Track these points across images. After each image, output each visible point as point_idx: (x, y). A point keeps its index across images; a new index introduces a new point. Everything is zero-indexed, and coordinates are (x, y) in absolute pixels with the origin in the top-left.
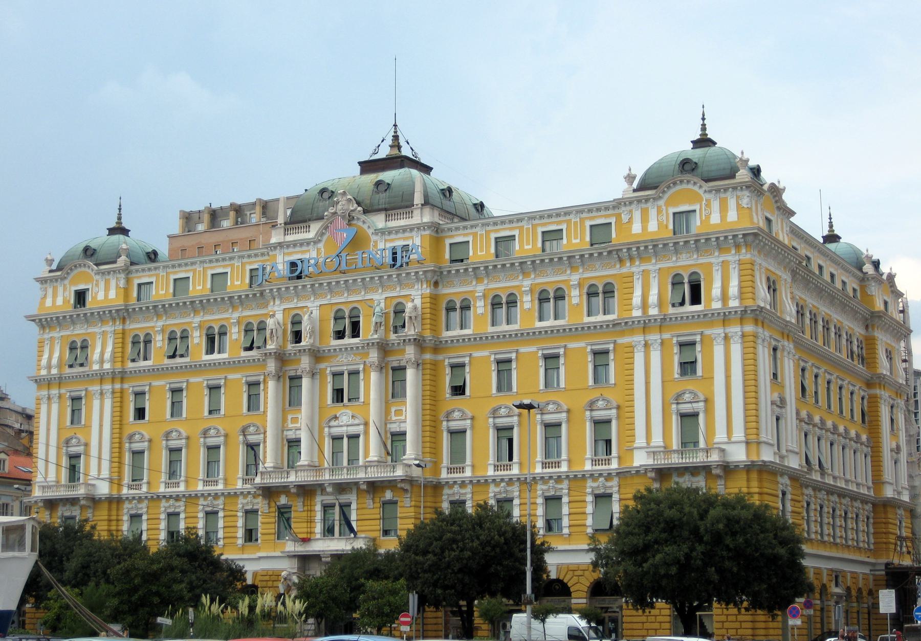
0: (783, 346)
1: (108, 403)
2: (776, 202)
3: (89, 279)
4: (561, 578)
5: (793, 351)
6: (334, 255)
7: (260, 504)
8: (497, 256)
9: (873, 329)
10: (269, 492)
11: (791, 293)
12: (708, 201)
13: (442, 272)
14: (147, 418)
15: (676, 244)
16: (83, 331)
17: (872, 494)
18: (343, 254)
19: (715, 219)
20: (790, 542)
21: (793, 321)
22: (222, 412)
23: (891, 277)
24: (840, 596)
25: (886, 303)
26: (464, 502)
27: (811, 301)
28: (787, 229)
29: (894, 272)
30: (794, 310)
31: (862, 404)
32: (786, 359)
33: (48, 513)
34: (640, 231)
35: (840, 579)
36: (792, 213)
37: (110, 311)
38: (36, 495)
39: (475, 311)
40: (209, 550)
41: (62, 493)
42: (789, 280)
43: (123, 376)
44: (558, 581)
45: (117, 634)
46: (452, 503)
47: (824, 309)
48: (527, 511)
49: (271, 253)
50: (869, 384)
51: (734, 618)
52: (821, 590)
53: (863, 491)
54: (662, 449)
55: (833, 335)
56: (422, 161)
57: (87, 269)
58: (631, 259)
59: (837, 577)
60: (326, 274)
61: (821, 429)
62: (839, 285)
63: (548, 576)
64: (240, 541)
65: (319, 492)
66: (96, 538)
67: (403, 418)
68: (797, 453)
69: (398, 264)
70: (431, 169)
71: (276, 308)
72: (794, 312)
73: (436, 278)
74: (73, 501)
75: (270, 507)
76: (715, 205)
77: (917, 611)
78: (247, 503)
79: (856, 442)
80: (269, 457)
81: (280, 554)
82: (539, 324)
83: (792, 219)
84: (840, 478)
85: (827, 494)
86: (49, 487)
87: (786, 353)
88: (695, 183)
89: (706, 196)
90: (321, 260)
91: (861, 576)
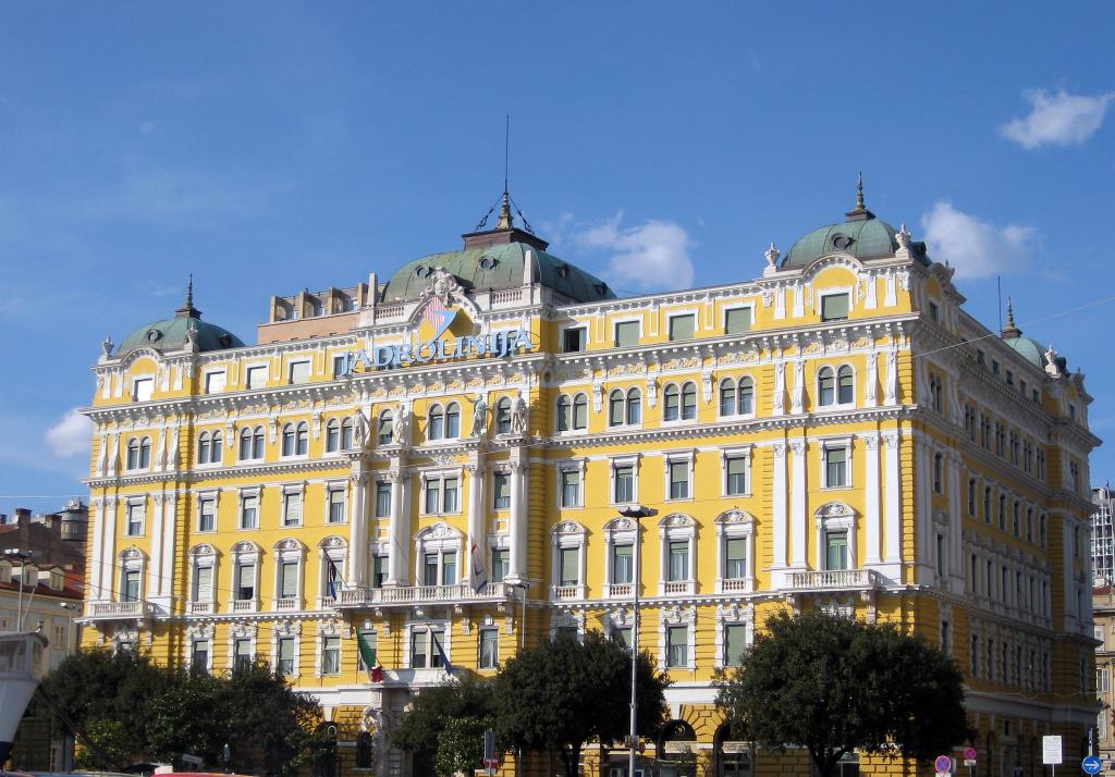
0: (948, 453)
1: (170, 509)
2: (943, 285)
3: (850, 279)
4: (685, 719)
5: (960, 460)
6: (432, 341)
7: (342, 628)
8: (671, 338)
9: (1057, 439)
10: (354, 616)
11: (959, 392)
12: (103, 379)
13: (554, 363)
14: (748, 490)
15: (824, 333)
16: (145, 428)
17: (1051, 628)
18: (441, 341)
19: (870, 304)
20: (949, 678)
21: (961, 424)
22: (300, 522)
23: (1079, 379)
24: (1009, 746)
25: (1072, 408)
26: (576, 629)
27: (983, 403)
28: (955, 317)
29: (1082, 372)
30: (962, 415)
31: (1042, 525)
32: (951, 468)
33: (102, 635)
34: (108, 397)
35: (1011, 726)
36: (962, 300)
37: (175, 405)
38: (88, 615)
39: (592, 409)
40: (280, 680)
41: (118, 614)
42: (957, 377)
43: (810, 422)
44: (681, 722)
45: (195, 768)
46: (561, 629)
47: (998, 413)
48: (649, 640)
49: (358, 339)
50: (1049, 502)
51: (882, 769)
52: (988, 738)
53: (1041, 624)
54: (394, 587)
55: (1008, 443)
56: (537, 236)
57: (146, 357)
58: (772, 349)
59: (1007, 723)
60: (421, 364)
61: (992, 551)
62: (1017, 385)
63: (668, 715)
64: (318, 673)
65: (408, 617)
66: (151, 663)
67: (507, 530)
68: (962, 578)
69: (504, 352)
71: (363, 403)
72: (962, 416)
73: (547, 370)
74: (129, 624)
75: (352, 633)
76: (871, 287)
77: (1086, 762)
78: (672, 616)
79: (1033, 568)
80: (349, 576)
81: (362, 687)
82: (239, 463)
83: (961, 307)
84: (999, 605)
85: (1012, 631)
86: (105, 606)
87: (950, 462)
88: (848, 262)
90: (415, 348)
91: (1021, 722)
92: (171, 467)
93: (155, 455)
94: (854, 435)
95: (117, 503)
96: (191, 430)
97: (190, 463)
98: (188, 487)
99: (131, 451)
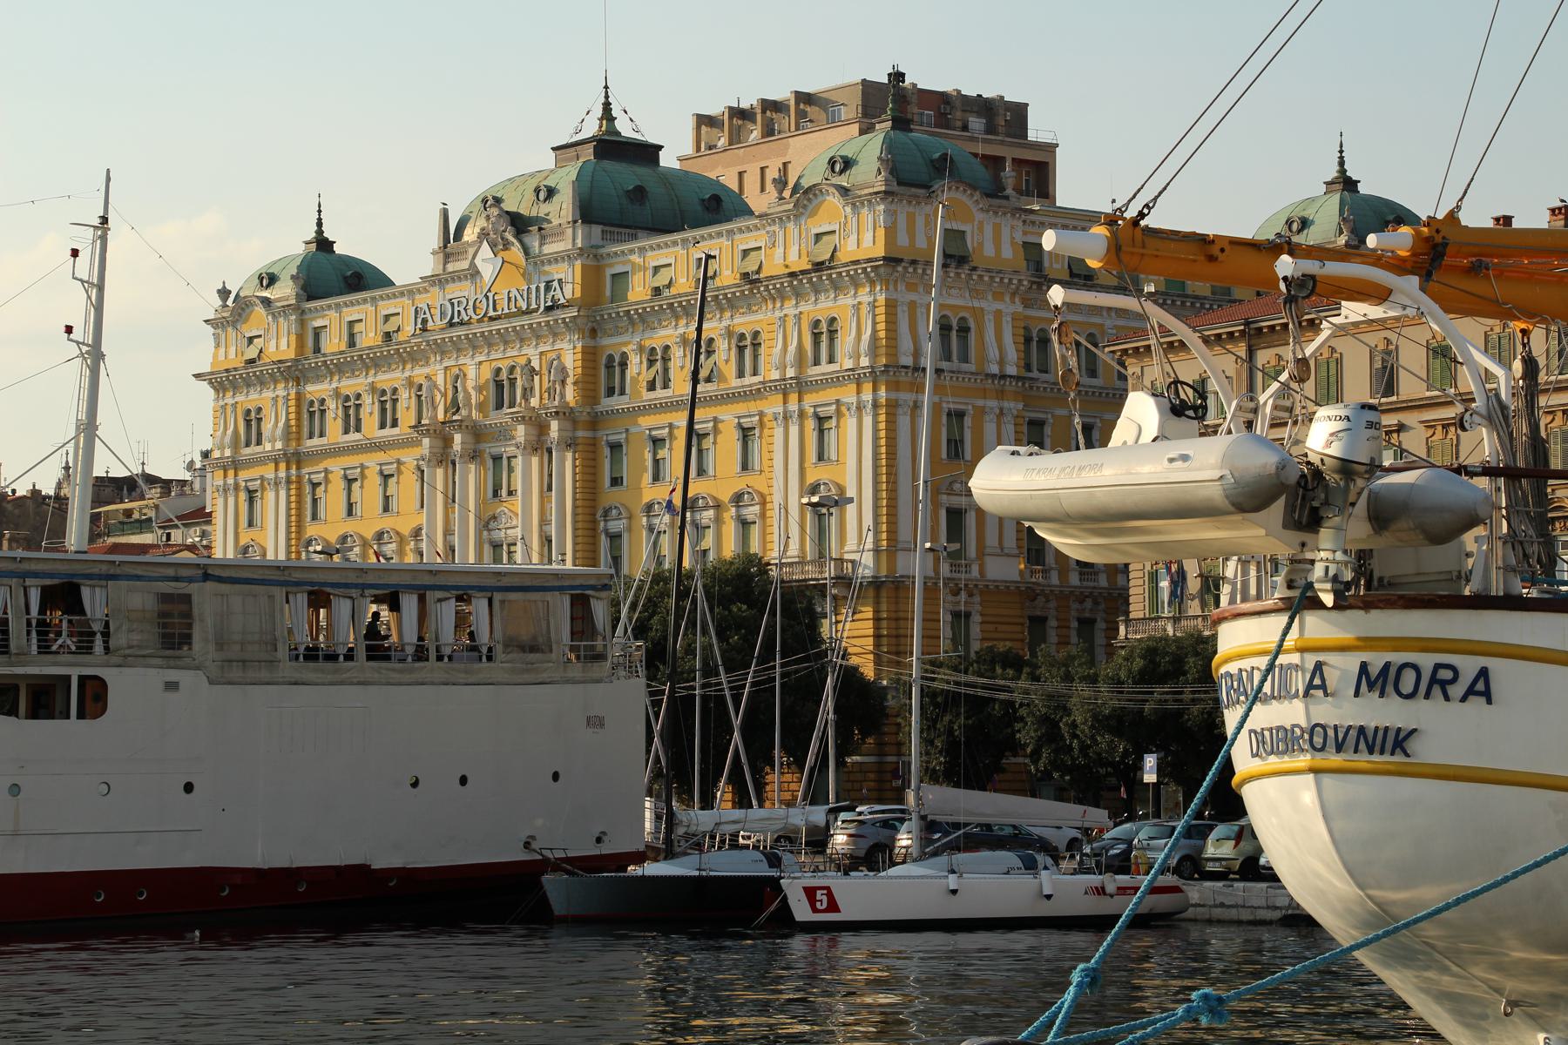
16: (830, 304)
70: (660, 147)
76: (988, 231)
89: (979, 216)
92: (865, 362)
93: (845, 342)
94: (838, 401)
95: (802, 414)
96: (298, 395)
97: (299, 439)
98: (298, 468)
99: (816, 337)
